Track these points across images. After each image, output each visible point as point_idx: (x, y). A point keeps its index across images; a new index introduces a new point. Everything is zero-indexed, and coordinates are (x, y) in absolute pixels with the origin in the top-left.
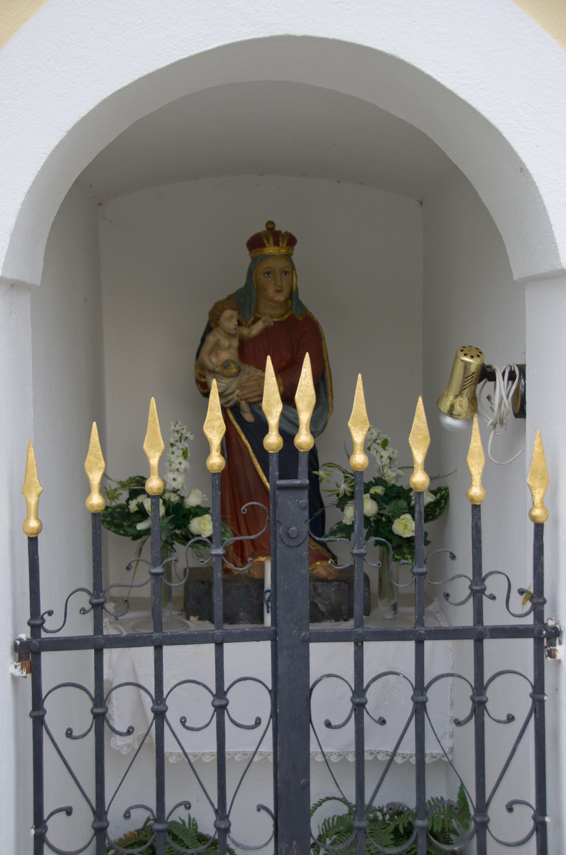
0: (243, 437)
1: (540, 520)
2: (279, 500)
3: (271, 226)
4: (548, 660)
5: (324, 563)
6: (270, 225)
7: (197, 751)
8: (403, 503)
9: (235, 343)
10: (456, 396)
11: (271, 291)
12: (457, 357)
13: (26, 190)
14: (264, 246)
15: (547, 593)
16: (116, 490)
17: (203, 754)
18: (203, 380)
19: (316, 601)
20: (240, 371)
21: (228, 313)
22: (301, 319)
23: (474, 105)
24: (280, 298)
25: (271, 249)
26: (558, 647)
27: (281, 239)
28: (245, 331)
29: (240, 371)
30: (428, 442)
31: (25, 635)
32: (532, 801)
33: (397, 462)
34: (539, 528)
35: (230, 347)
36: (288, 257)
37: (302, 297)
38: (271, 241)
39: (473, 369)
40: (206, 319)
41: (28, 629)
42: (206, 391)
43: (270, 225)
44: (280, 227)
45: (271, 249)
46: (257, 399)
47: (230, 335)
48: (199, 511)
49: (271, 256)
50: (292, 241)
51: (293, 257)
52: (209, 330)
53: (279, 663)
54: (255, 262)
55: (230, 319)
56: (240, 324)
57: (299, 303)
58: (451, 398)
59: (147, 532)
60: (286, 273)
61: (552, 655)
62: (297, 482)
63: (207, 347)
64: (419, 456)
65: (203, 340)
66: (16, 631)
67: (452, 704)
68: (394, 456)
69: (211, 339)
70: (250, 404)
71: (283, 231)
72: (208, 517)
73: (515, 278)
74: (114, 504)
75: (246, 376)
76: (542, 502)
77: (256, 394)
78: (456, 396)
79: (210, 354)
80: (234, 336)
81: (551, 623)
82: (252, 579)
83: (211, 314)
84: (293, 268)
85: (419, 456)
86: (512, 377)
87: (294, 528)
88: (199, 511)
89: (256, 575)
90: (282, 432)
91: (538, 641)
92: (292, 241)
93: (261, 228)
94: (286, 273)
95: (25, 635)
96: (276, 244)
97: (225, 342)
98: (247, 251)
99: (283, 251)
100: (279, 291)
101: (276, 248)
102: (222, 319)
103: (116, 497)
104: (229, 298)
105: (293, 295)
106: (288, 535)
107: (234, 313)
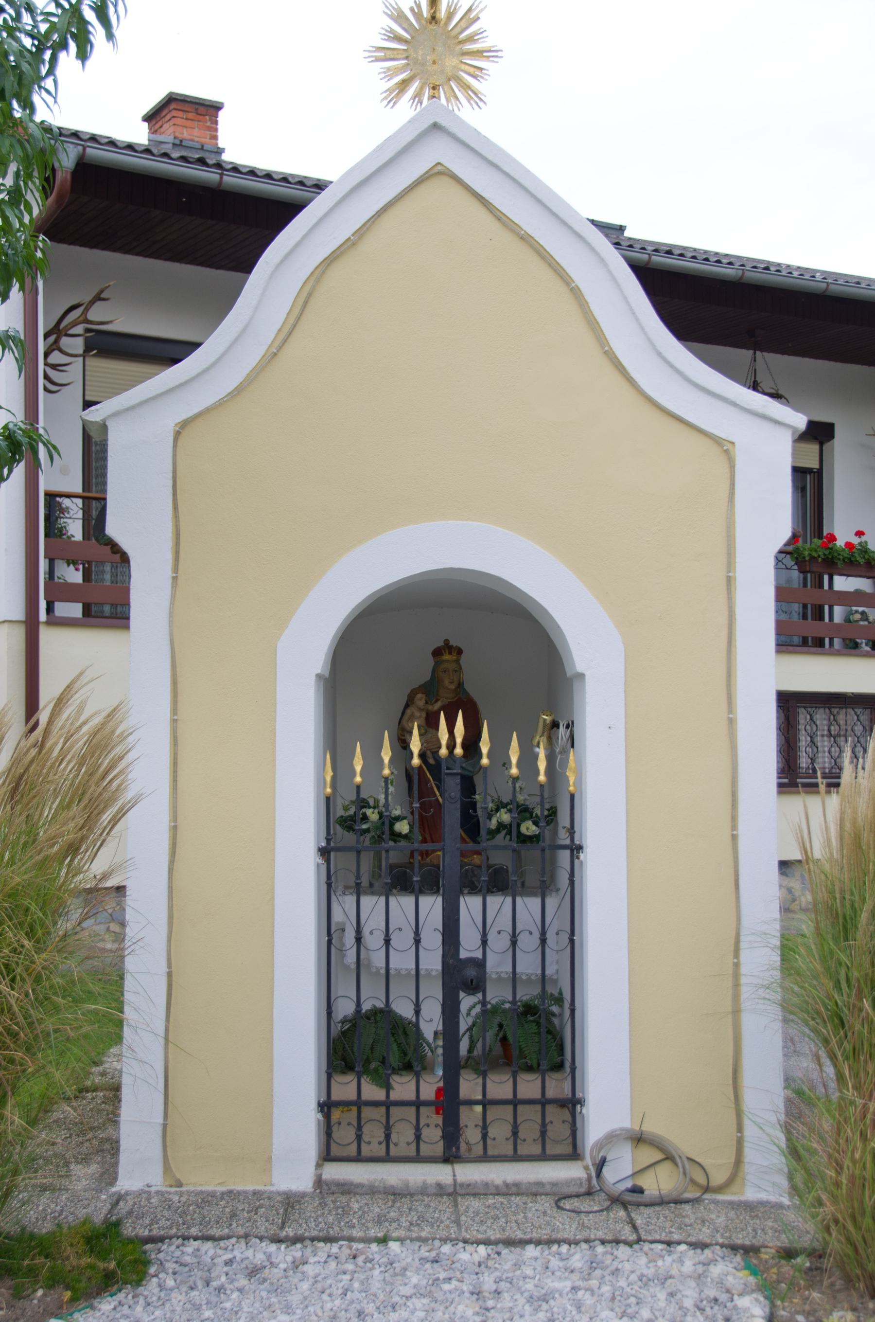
0: (428, 774)
1: (573, 792)
2: (446, 780)
3: (447, 642)
4: (576, 861)
5: (479, 857)
6: (447, 642)
7: (397, 967)
8: (528, 815)
9: (424, 715)
10: (541, 737)
11: (446, 682)
12: (540, 716)
13: (333, 634)
14: (442, 654)
15: (576, 829)
16: (348, 805)
17: (401, 969)
18: (403, 738)
19: (473, 879)
20: (426, 732)
21: (419, 696)
22: (465, 700)
23: (536, 599)
24: (453, 687)
25: (446, 657)
26: (581, 854)
27: (453, 650)
28: (430, 707)
29: (426, 732)
30: (518, 753)
31: (323, 844)
32: (568, 930)
33: (525, 791)
34: (572, 796)
35: (420, 717)
36: (457, 661)
37: (466, 686)
38: (447, 652)
39: (548, 722)
40: (406, 699)
41: (325, 841)
42: (404, 745)
43: (447, 642)
44: (453, 643)
45: (446, 657)
46: (437, 750)
47: (420, 710)
48: (398, 819)
49: (447, 661)
50: (460, 652)
51: (461, 662)
52: (407, 706)
53: (446, 859)
54: (437, 665)
55: (421, 699)
56: (427, 703)
57: (465, 690)
58: (538, 737)
59: (367, 831)
60: (456, 671)
61: (578, 858)
62: (455, 771)
63: (406, 717)
64: (514, 760)
65: (403, 713)
66: (318, 841)
67: (557, 942)
68: (523, 786)
69: (409, 711)
70: (433, 753)
71: (454, 646)
72: (405, 822)
73: (568, 675)
74: (347, 814)
75: (430, 736)
76: (574, 783)
77: (436, 746)
78: (541, 737)
79: (408, 721)
80: (423, 710)
81: (578, 843)
82: (433, 866)
83: (409, 696)
84: (461, 668)
85: (514, 760)
86: (568, 727)
87: (453, 794)
88: (398, 819)
89: (435, 862)
90: (448, 748)
91: (572, 851)
92: (460, 652)
93: (441, 643)
94: (456, 671)
95: (323, 844)
96: (450, 653)
97: (417, 714)
98: (432, 658)
99: (455, 658)
100: (451, 683)
101: (450, 656)
102: (416, 699)
103: (349, 809)
104: (420, 686)
105: (460, 685)
106: (450, 797)
107: (424, 696)
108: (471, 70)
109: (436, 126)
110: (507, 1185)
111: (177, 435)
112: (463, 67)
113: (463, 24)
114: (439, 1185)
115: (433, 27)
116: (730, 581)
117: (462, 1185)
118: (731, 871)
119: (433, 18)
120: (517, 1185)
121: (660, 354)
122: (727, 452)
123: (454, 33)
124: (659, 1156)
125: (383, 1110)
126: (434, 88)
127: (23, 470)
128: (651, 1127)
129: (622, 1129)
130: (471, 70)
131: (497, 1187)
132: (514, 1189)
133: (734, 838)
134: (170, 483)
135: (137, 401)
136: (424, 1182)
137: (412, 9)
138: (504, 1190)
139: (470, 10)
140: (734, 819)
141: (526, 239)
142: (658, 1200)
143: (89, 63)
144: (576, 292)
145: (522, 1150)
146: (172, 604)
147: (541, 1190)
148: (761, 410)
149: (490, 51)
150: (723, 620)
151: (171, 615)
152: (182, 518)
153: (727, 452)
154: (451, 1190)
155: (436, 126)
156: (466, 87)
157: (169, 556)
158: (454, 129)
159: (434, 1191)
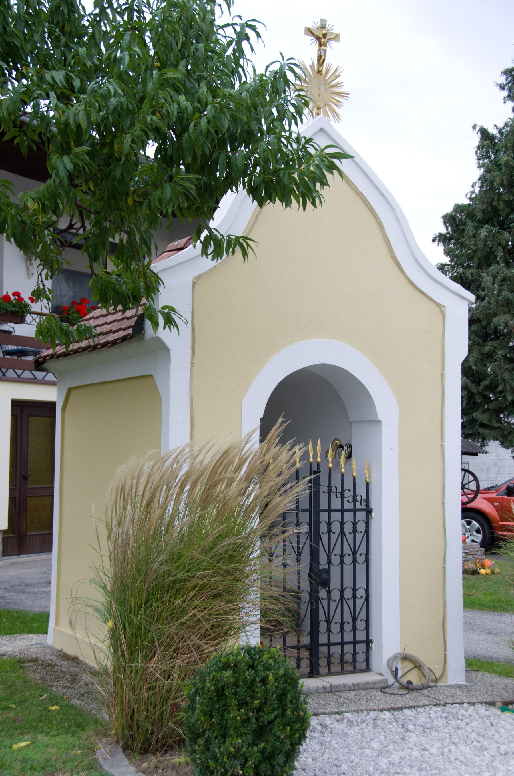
108: (335, 102)
109: (322, 130)
110: (353, 685)
111: (194, 283)
112: (332, 100)
113: (333, 77)
114: (324, 688)
115: (319, 77)
116: (443, 376)
117: (334, 687)
118: (442, 521)
119: (319, 72)
120: (358, 685)
121: (416, 260)
122: (442, 311)
123: (328, 81)
124: (411, 666)
125: (340, 647)
126: (318, 109)
127: (160, 303)
128: (409, 651)
129: (398, 653)
130: (335, 102)
131: (349, 687)
132: (357, 687)
133: (443, 504)
134: (191, 310)
135: (175, 264)
136: (317, 687)
137: (310, 66)
138: (353, 688)
139: (336, 71)
140: (444, 495)
141: (359, 194)
142: (422, 687)
143: (476, 139)
144: (380, 224)
145: (333, 669)
146: (191, 378)
147: (368, 687)
148: (457, 292)
149: (344, 93)
150: (439, 396)
151: (191, 385)
152: (196, 330)
153: (442, 311)
154: (329, 690)
155: (322, 130)
156: (333, 111)
157: (190, 351)
158: (331, 133)
159: (322, 691)
